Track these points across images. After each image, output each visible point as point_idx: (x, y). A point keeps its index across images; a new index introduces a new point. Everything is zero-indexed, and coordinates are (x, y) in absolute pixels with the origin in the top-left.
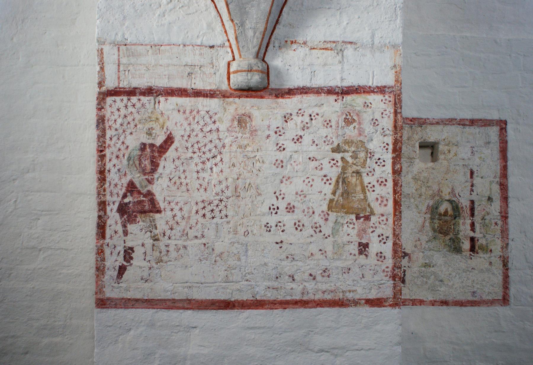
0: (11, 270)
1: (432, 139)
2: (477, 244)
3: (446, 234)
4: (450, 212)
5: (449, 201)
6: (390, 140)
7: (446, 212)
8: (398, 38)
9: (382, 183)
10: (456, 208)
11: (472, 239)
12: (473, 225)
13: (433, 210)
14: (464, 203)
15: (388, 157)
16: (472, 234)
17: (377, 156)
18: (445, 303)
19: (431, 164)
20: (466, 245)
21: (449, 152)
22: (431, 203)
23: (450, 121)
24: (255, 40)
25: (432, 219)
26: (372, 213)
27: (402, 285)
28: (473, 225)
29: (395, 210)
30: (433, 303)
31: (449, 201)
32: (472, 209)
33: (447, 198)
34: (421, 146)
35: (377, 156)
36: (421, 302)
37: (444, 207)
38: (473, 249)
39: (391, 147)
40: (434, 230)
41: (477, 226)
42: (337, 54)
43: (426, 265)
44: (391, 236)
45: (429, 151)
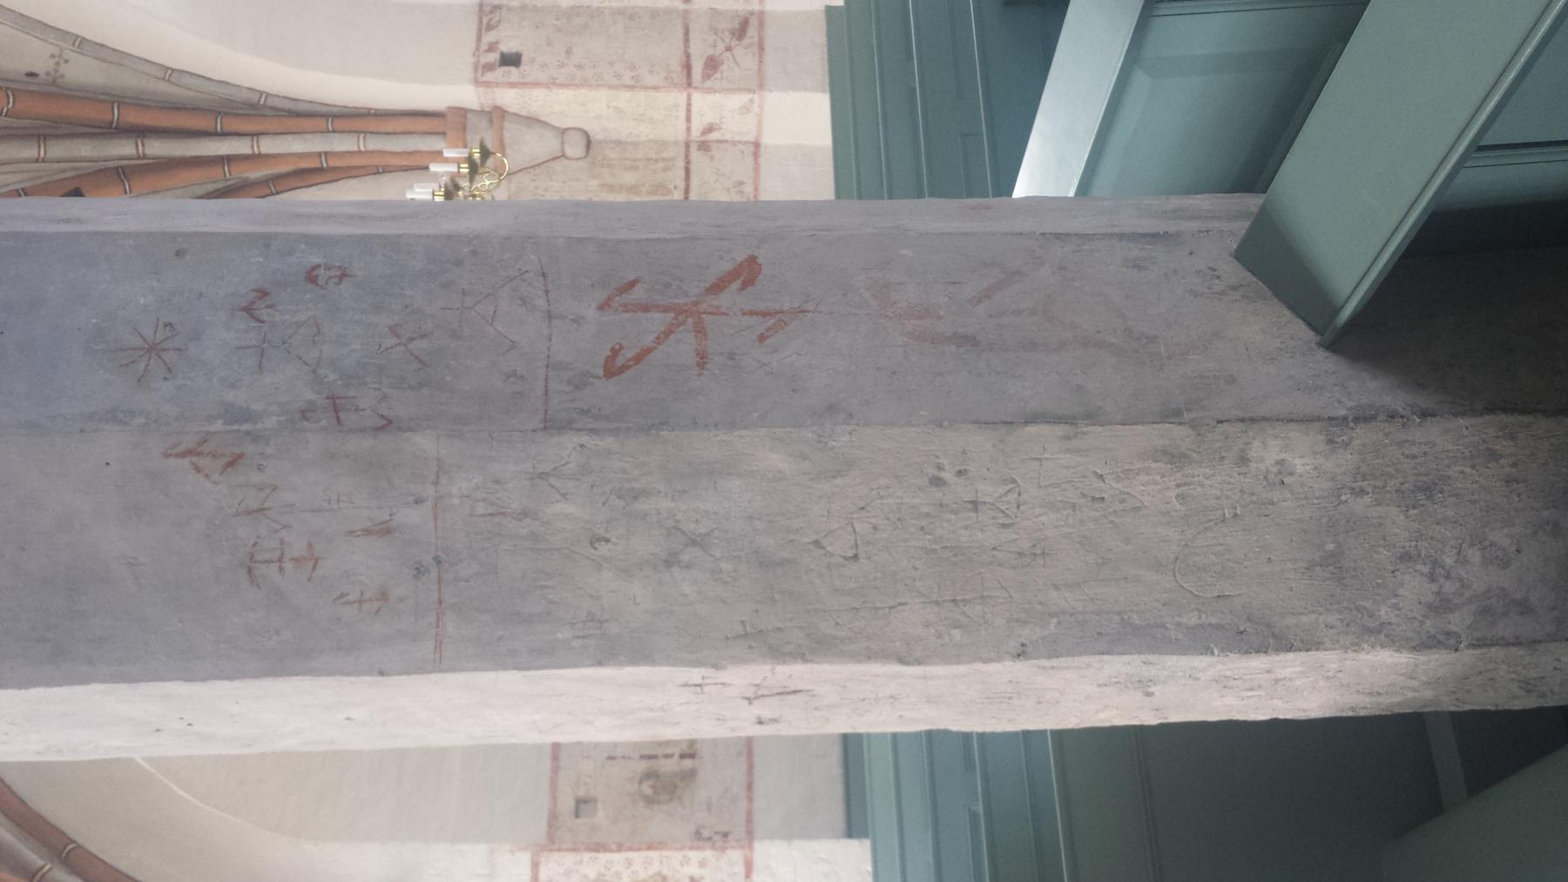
0: (743, 282)
1: (572, 804)
2: (687, 751)
3: (675, 787)
4: (652, 782)
5: (641, 782)
6: (586, 856)
7: (653, 787)
8: (482, 848)
9: (629, 863)
10: (650, 775)
11: (682, 756)
12: (667, 756)
13: (650, 801)
14: (642, 766)
15: (603, 857)
16: (676, 757)
17: (602, 870)
18: (750, 786)
19: (599, 805)
20: (688, 763)
21: (586, 784)
22: (642, 804)
23: (553, 783)
24: (1291, 434)
25: (659, 802)
26: (659, 874)
27: (325, 395)
28: (667, 756)
29: (657, 849)
30: (750, 799)
31: (641, 782)
32: (651, 757)
33: (636, 786)
34: (577, 816)
35: (602, 870)
36: (749, 813)
37: (647, 789)
38: (692, 756)
39: (594, 855)
40: (671, 800)
41: (669, 751)
42: (1371, 617)
43: (709, 809)
44: (683, 853)
45: (583, 806)
